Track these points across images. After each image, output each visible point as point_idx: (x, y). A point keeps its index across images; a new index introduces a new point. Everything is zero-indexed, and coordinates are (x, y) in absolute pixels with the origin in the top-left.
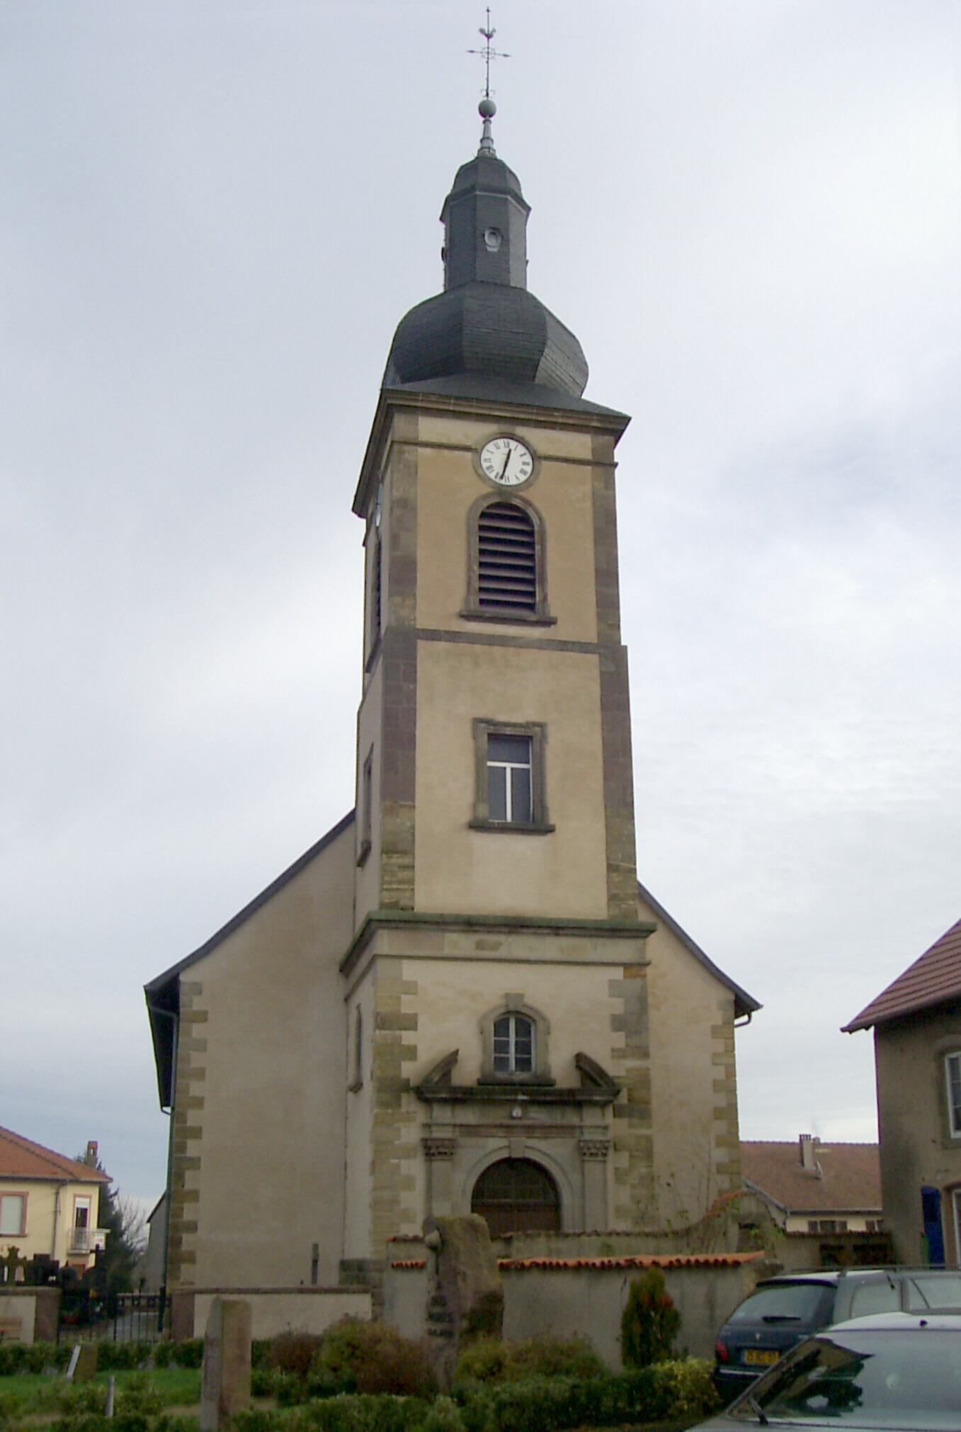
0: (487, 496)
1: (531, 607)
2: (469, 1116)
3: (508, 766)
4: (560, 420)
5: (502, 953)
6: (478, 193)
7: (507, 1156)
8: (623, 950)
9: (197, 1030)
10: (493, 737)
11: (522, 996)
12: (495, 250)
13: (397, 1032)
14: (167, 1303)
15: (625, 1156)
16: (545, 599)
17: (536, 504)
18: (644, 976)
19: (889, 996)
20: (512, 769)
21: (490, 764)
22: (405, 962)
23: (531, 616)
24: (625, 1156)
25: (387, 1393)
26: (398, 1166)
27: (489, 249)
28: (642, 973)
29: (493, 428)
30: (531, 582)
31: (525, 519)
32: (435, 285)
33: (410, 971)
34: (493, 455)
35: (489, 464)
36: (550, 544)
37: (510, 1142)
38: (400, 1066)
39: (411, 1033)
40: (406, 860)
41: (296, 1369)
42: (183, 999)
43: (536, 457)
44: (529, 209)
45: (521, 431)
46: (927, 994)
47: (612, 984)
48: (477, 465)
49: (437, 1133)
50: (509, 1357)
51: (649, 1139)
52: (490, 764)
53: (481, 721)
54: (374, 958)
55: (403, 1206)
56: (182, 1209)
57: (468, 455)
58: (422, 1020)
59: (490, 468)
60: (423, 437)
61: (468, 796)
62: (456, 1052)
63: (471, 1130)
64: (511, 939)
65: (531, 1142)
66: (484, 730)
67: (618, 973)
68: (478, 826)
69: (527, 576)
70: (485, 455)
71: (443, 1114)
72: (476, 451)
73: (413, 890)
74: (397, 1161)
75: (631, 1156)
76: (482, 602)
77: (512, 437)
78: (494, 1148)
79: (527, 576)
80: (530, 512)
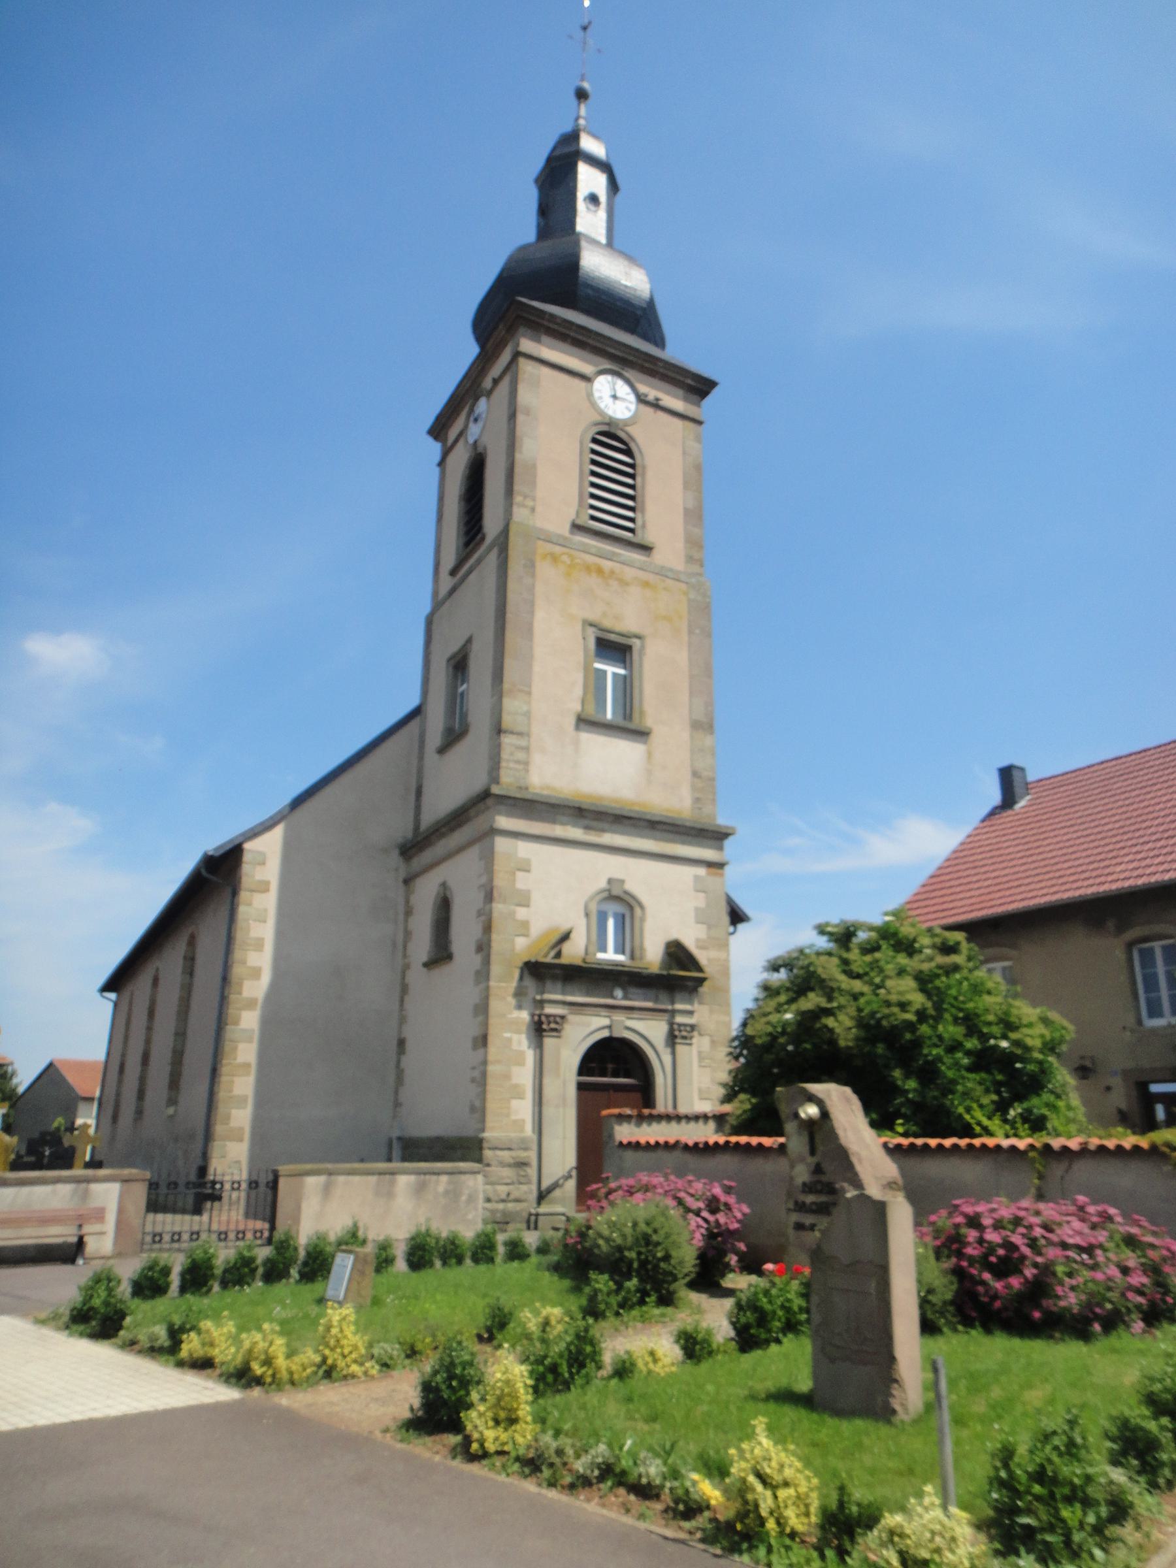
4: (661, 370)
11: (622, 882)
13: (513, 907)
14: (814, 1426)
15: (706, 1041)
19: (934, 880)
20: (615, 675)
24: (706, 1041)
26: (509, 1040)
31: (628, 452)
36: (650, 474)
37: (612, 1021)
38: (513, 941)
40: (523, 742)
41: (400, 1252)
45: (629, 373)
46: (942, 896)
47: (697, 878)
50: (191, 1345)
53: (591, 625)
54: (517, 354)
61: (578, 691)
67: (702, 871)
68: (584, 722)
69: (630, 503)
79: (630, 503)
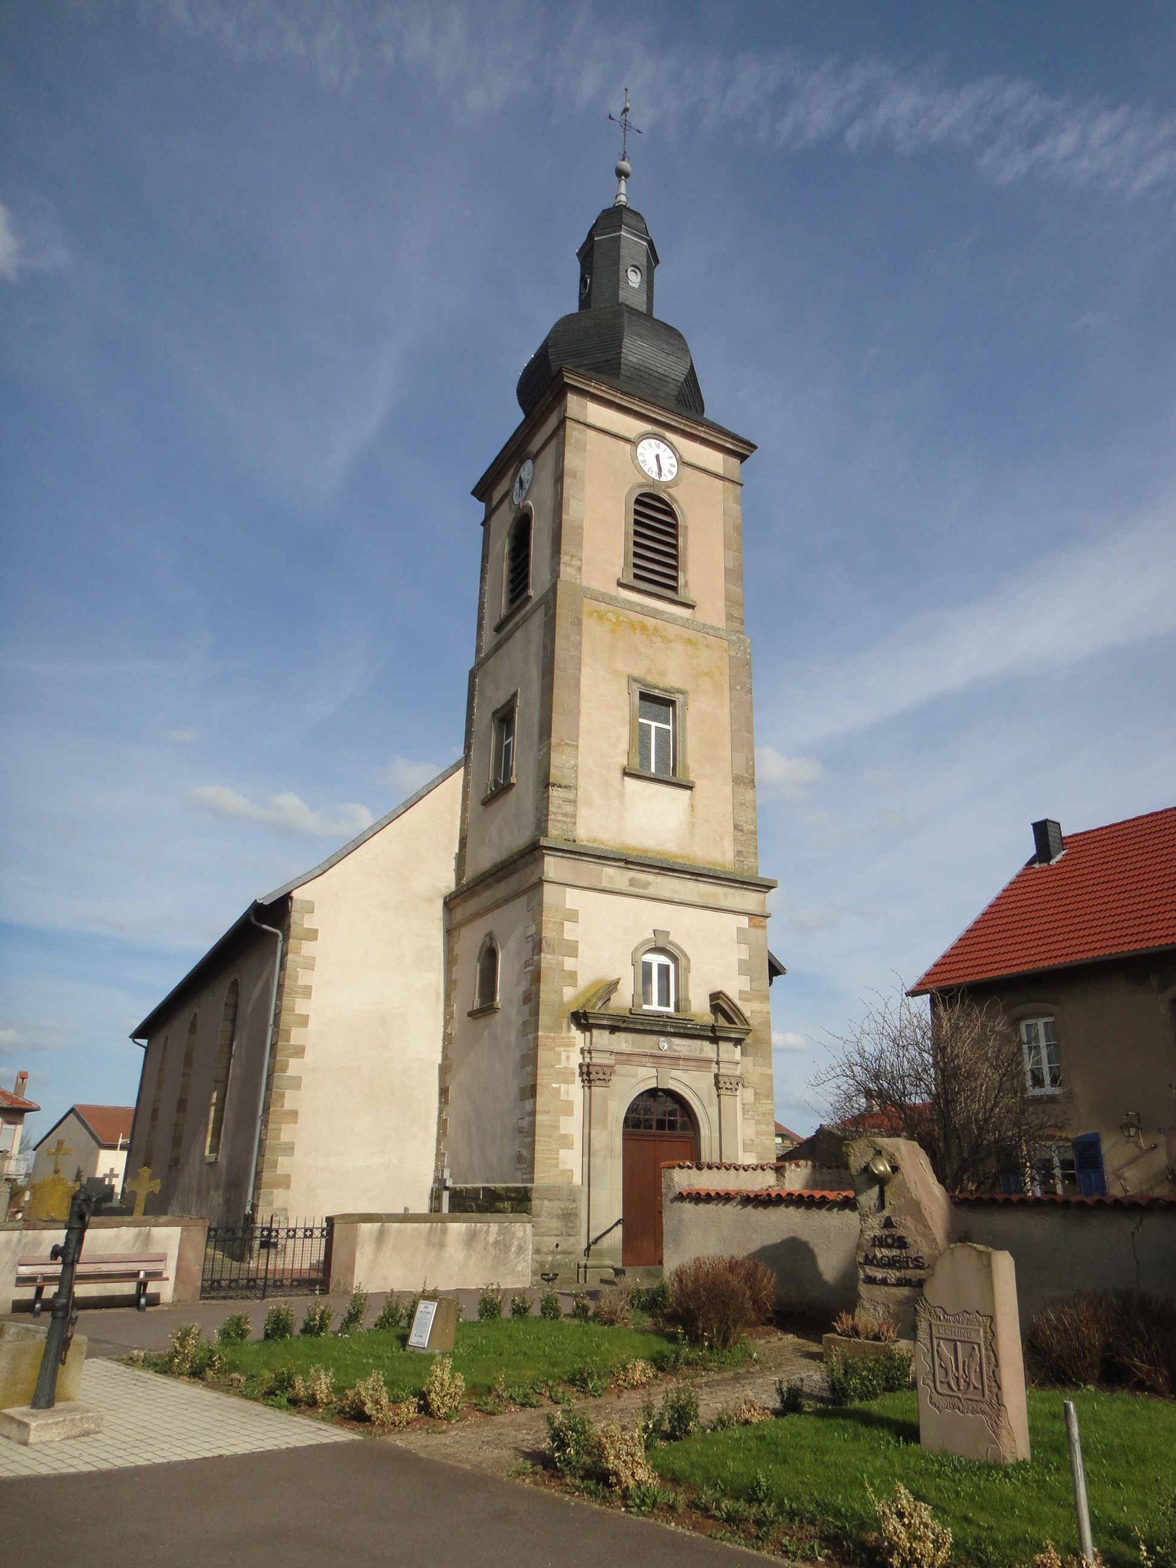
0: (641, 486)
1: (674, 589)
2: (623, 1042)
3: (654, 724)
5: (650, 891)
6: (622, 233)
7: (655, 1086)
8: (749, 900)
9: (307, 948)
10: (644, 696)
12: (636, 286)
13: (561, 958)
16: (686, 585)
17: (680, 502)
18: (764, 927)
21: (641, 720)
22: (568, 890)
23: (669, 593)
25: (878, 1278)
26: (558, 1090)
27: (630, 284)
28: (763, 924)
29: (647, 427)
30: (675, 568)
31: (671, 514)
32: (572, 306)
33: (573, 899)
34: (649, 451)
35: (643, 459)
36: (691, 535)
38: (562, 991)
39: (573, 959)
42: (295, 916)
43: (683, 463)
44: (658, 262)
48: (634, 457)
49: (598, 1059)
51: (770, 1077)
52: (641, 720)
55: (562, 1132)
56: (280, 1130)
57: (628, 447)
58: (582, 948)
59: (644, 461)
60: (591, 420)
62: (619, 979)
63: (625, 1057)
64: (660, 879)
65: (675, 1073)
66: (636, 689)
67: (744, 921)
70: (640, 449)
71: (602, 1038)
72: (633, 443)
73: (575, 823)
74: (558, 1085)
75: (756, 1094)
76: (636, 576)
77: (662, 439)
78: (643, 1078)
80: (674, 506)
